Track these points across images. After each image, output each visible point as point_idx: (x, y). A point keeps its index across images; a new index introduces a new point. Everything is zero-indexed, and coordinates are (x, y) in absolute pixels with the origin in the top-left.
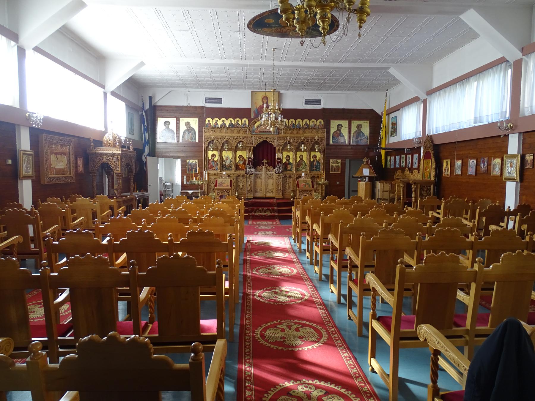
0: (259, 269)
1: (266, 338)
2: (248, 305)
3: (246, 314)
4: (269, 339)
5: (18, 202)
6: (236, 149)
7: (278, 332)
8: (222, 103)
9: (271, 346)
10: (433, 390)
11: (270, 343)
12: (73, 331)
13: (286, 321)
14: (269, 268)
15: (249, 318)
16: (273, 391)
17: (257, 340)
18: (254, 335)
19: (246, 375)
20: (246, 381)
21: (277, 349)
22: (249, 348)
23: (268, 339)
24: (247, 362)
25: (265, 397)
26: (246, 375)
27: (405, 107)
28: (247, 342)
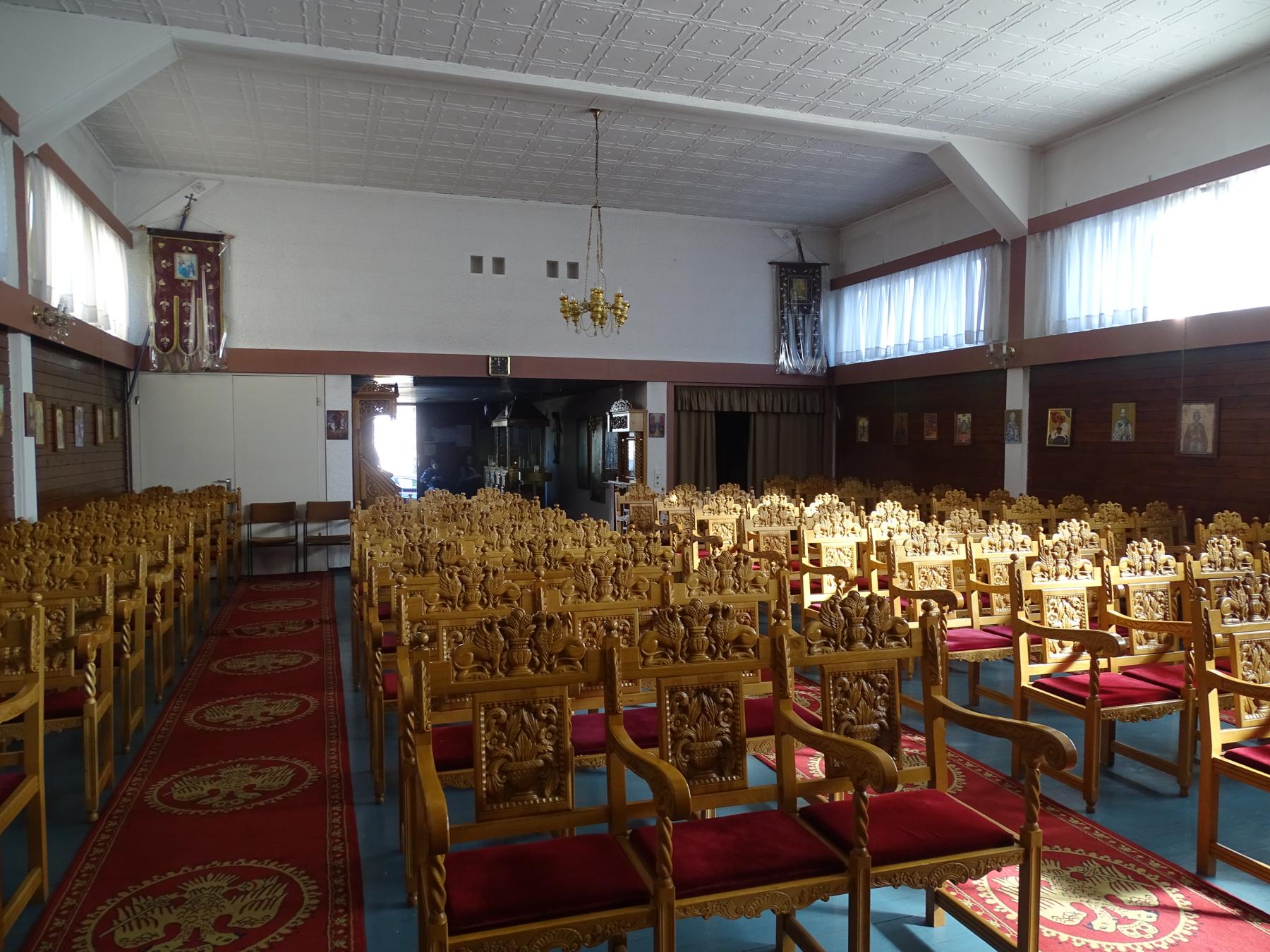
0: (294, 782)
1: (284, 886)
2: (335, 783)
3: (338, 761)
4: (277, 883)
5: (1002, 487)
6: (364, 538)
7: (241, 913)
8: (577, 263)
9: (276, 866)
10: (77, 687)
11: (286, 763)
12: (820, 796)
13: (232, 809)
14: (276, 668)
15: (334, 817)
16: (277, 937)
17: (310, 879)
18: (320, 894)
19: (345, 916)
20: (343, 884)
21: (261, 860)
22: (333, 838)
23: (278, 885)
24: (338, 824)
25: (302, 920)
26: (344, 896)
27: (1089, 221)
28: (338, 824)
